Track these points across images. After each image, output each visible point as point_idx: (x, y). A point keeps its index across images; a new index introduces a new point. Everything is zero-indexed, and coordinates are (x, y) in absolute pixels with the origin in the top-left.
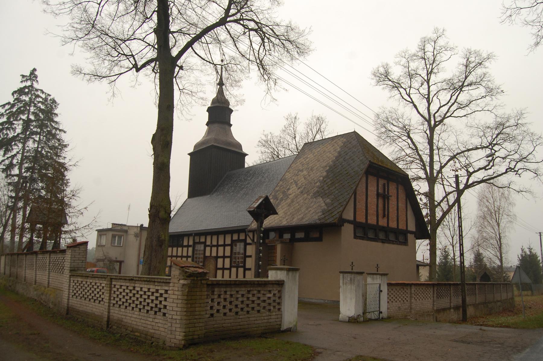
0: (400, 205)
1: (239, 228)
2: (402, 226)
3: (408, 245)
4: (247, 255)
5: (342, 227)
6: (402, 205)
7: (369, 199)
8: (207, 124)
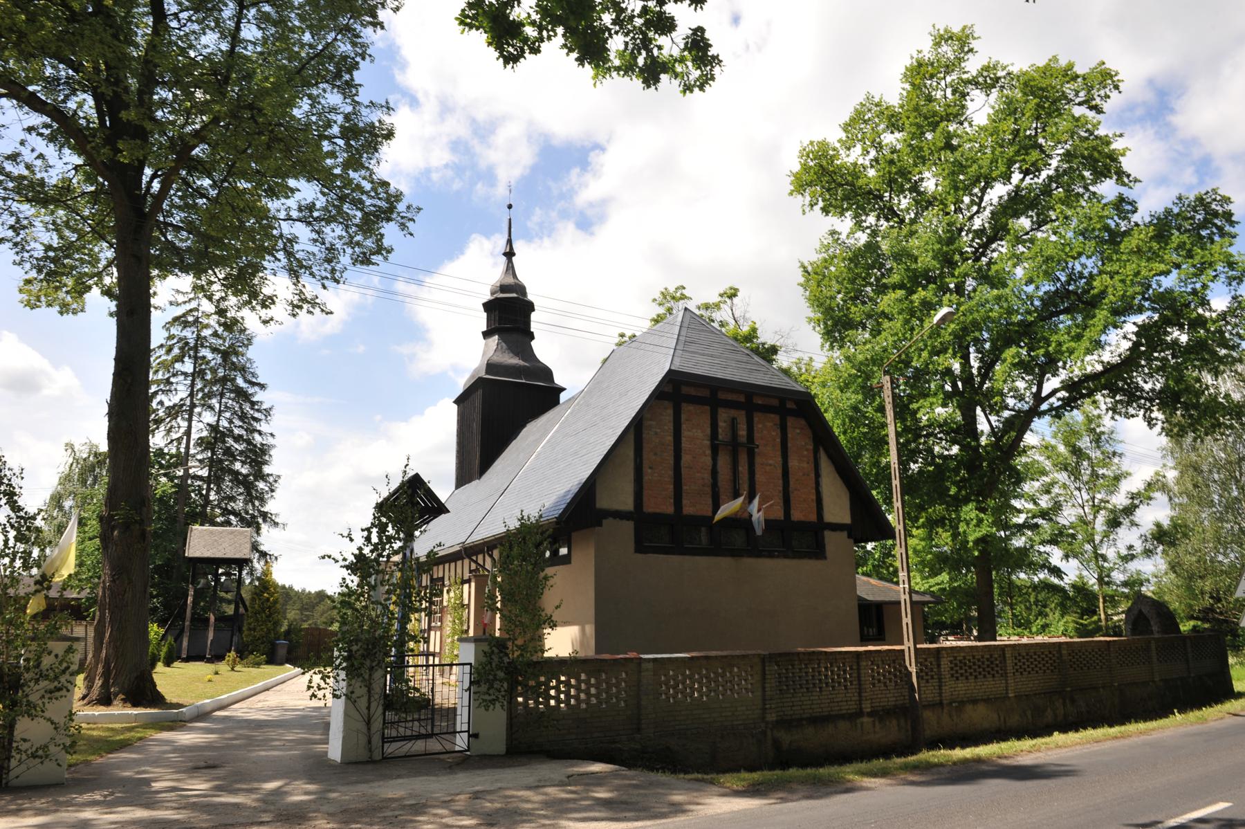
0: (793, 463)
2: (802, 512)
3: (825, 558)
4: (684, 405)
7: (686, 459)
8: (486, 335)
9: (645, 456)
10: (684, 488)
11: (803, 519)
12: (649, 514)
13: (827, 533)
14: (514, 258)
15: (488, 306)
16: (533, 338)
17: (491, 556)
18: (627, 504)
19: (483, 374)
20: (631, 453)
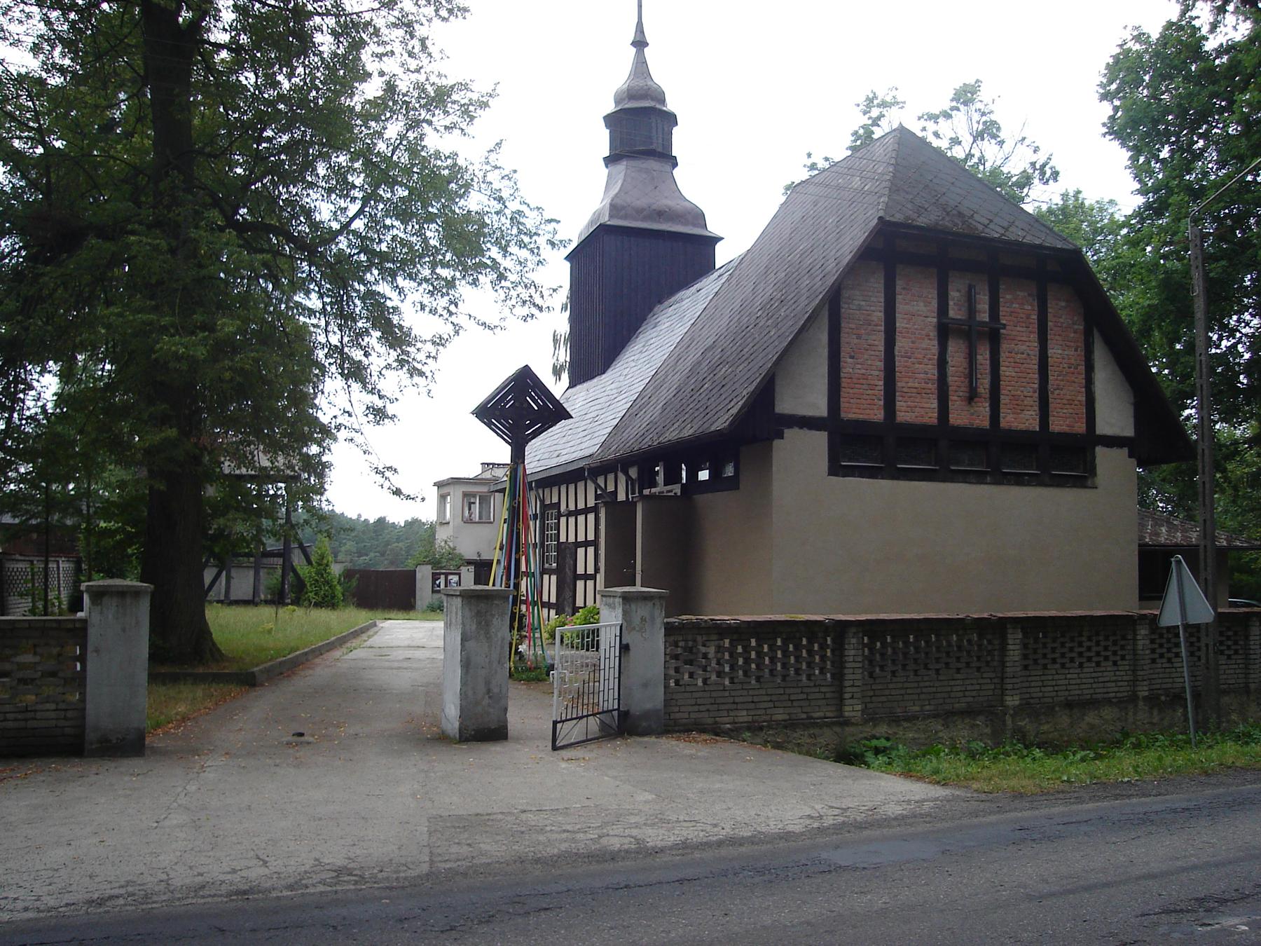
0: (1054, 352)
1: (554, 472)
2: (1064, 421)
5: (777, 443)
6: (1063, 353)
7: (901, 344)
8: (609, 161)
9: (844, 338)
10: (899, 384)
11: (1065, 429)
12: (850, 421)
13: (1099, 450)
14: (646, 50)
15: (610, 120)
16: (675, 165)
17: (626, 474)
18: (818, 406)
19: (605, 219)
20: (824, 338)
